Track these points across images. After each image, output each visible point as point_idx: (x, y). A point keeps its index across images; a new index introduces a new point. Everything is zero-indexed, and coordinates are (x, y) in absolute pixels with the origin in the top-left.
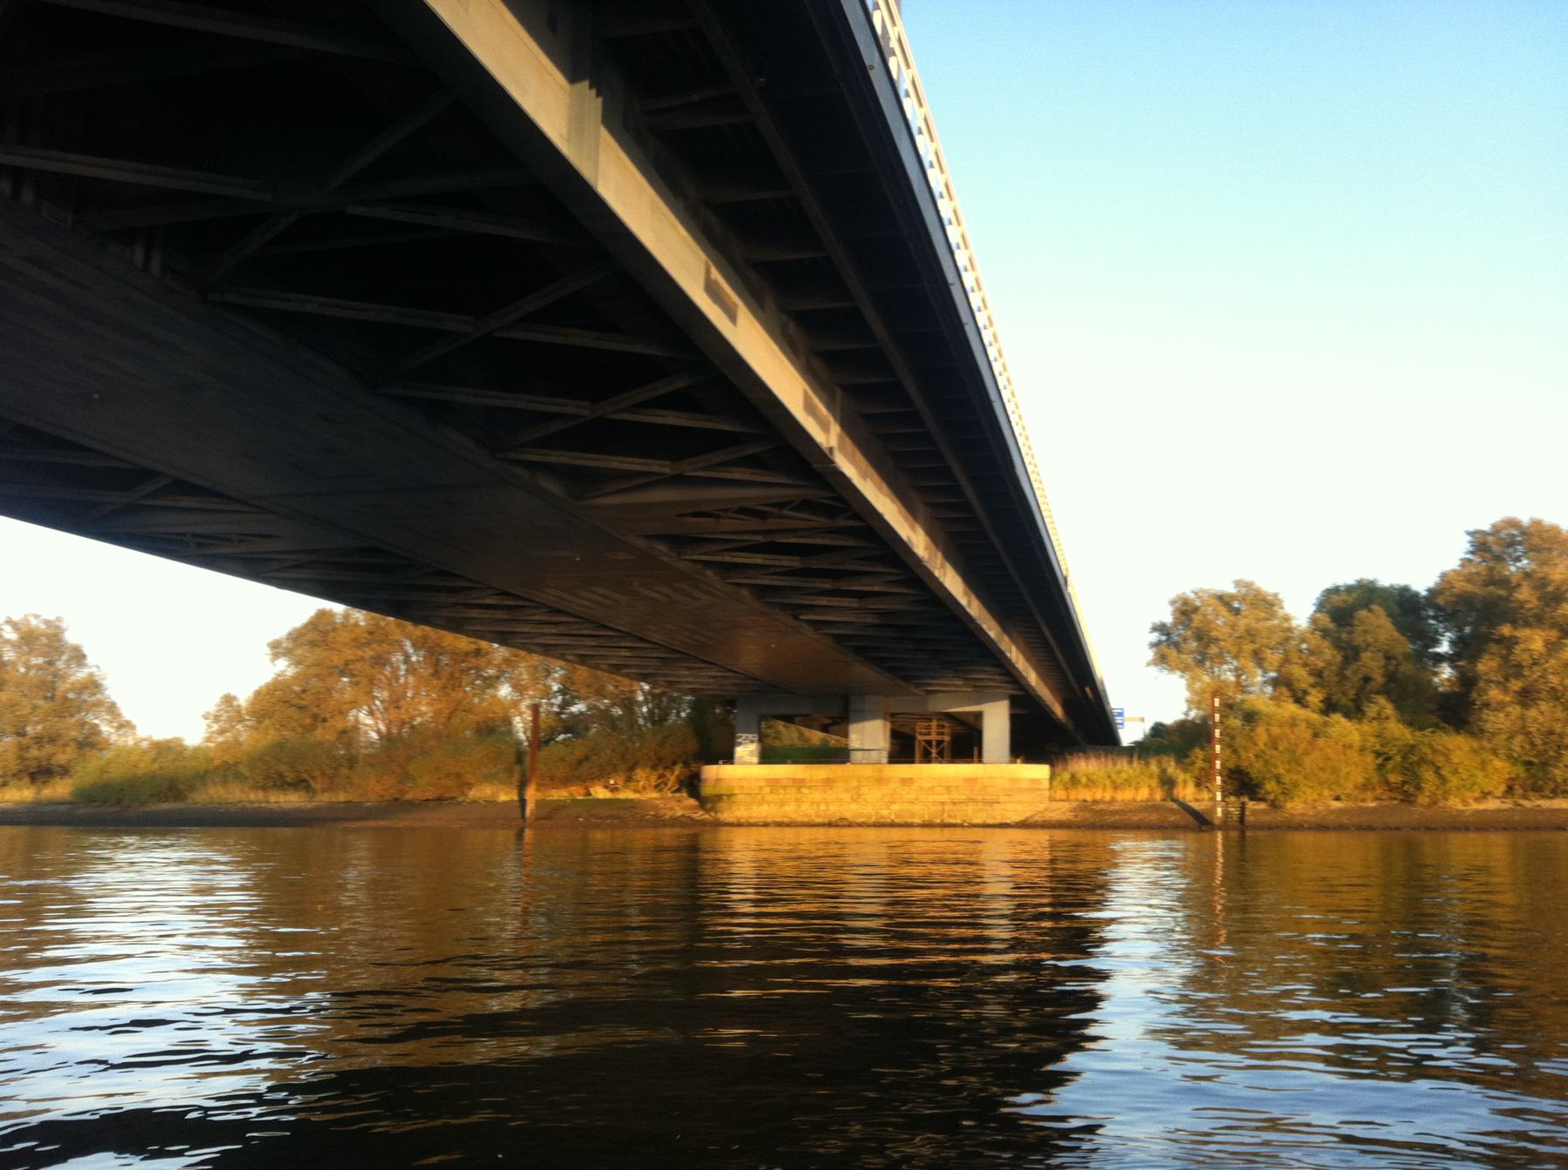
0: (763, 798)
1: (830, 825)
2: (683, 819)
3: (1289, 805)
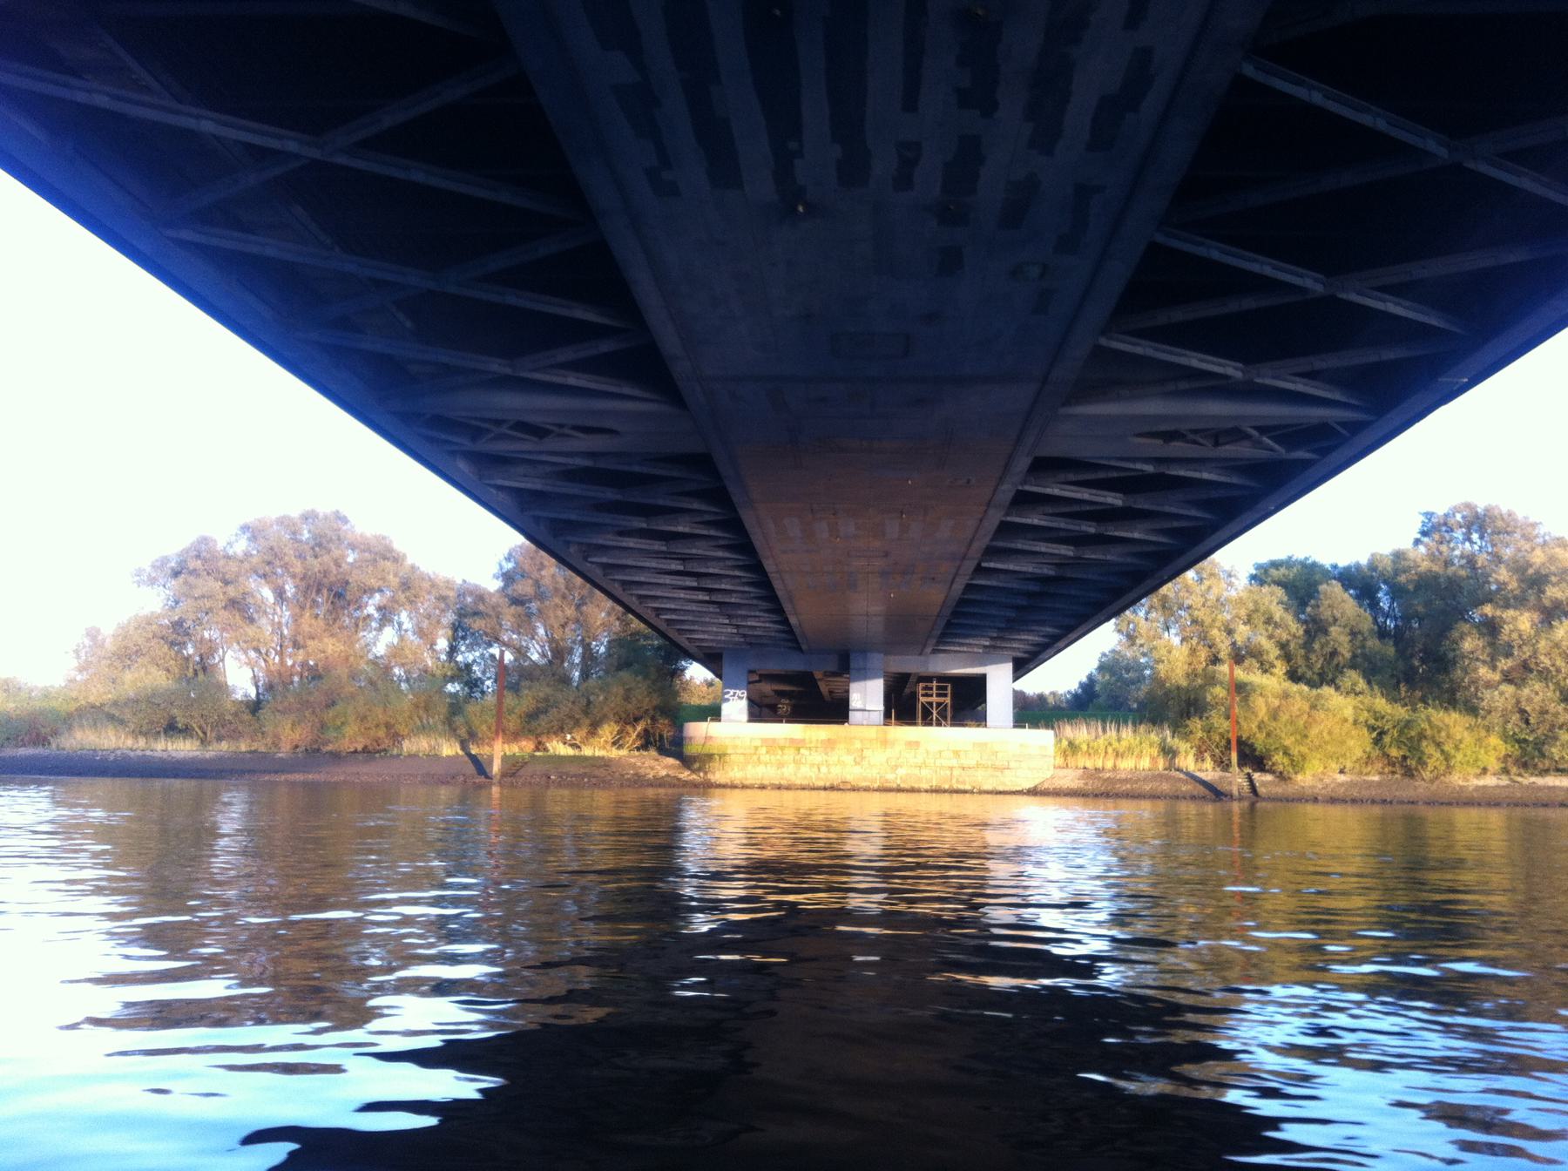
0: (759, 759)
1: (832, 788)
2: (669, 779)
3: (1299, 777)
